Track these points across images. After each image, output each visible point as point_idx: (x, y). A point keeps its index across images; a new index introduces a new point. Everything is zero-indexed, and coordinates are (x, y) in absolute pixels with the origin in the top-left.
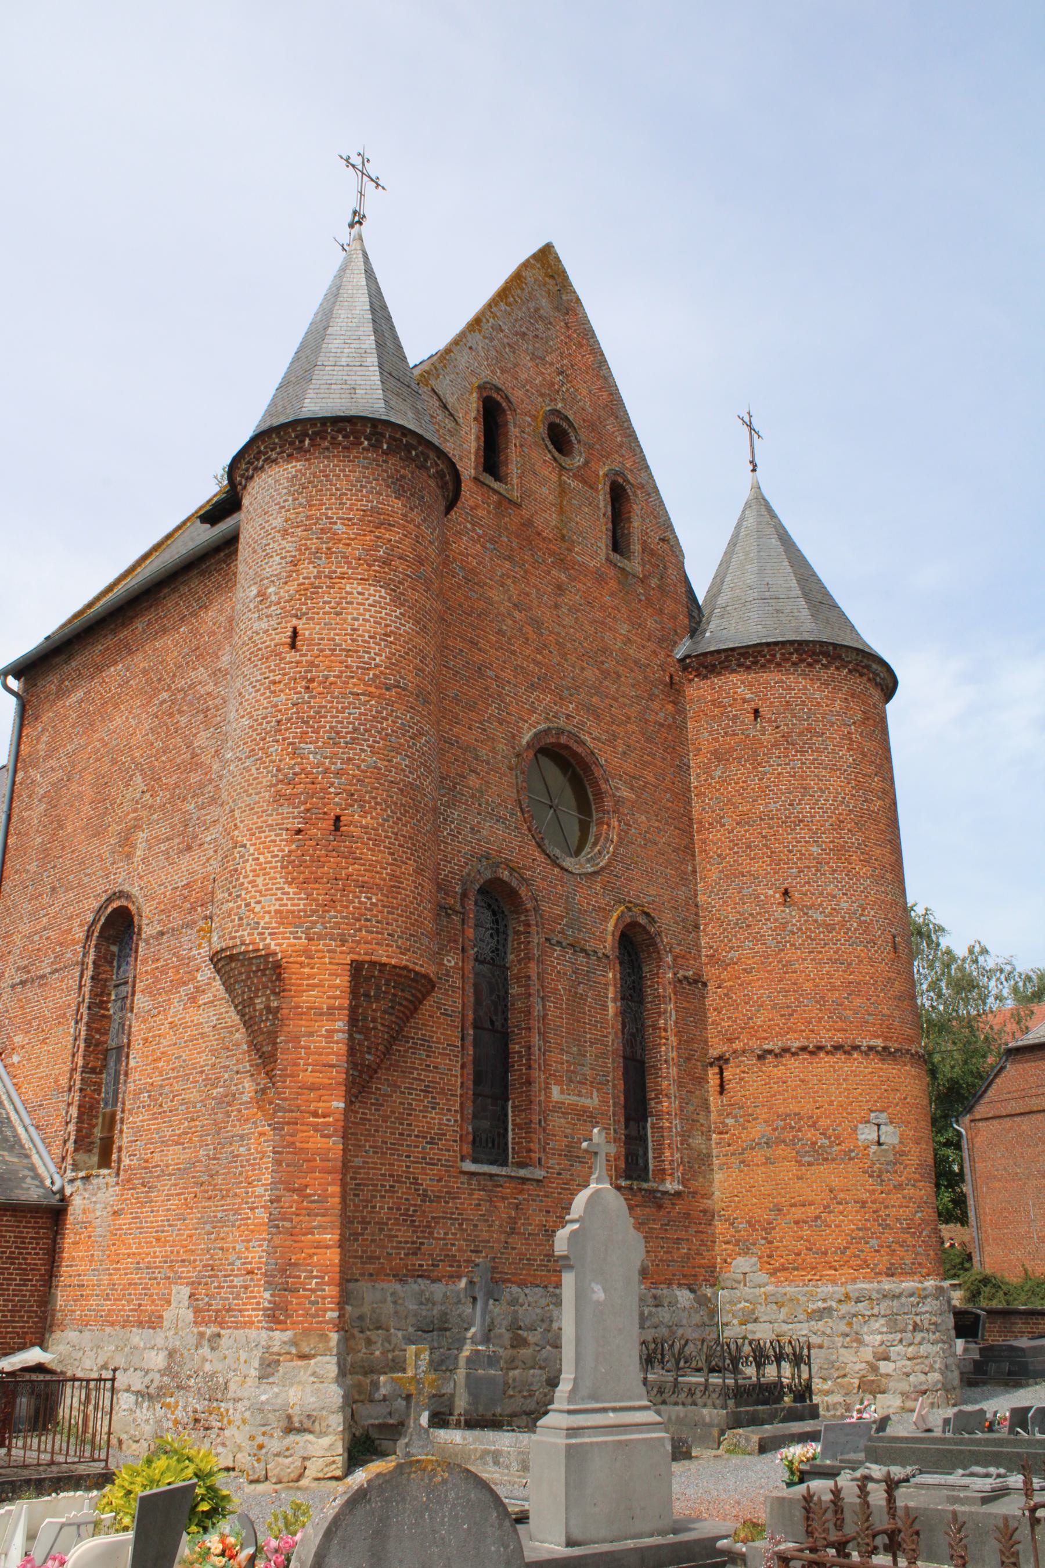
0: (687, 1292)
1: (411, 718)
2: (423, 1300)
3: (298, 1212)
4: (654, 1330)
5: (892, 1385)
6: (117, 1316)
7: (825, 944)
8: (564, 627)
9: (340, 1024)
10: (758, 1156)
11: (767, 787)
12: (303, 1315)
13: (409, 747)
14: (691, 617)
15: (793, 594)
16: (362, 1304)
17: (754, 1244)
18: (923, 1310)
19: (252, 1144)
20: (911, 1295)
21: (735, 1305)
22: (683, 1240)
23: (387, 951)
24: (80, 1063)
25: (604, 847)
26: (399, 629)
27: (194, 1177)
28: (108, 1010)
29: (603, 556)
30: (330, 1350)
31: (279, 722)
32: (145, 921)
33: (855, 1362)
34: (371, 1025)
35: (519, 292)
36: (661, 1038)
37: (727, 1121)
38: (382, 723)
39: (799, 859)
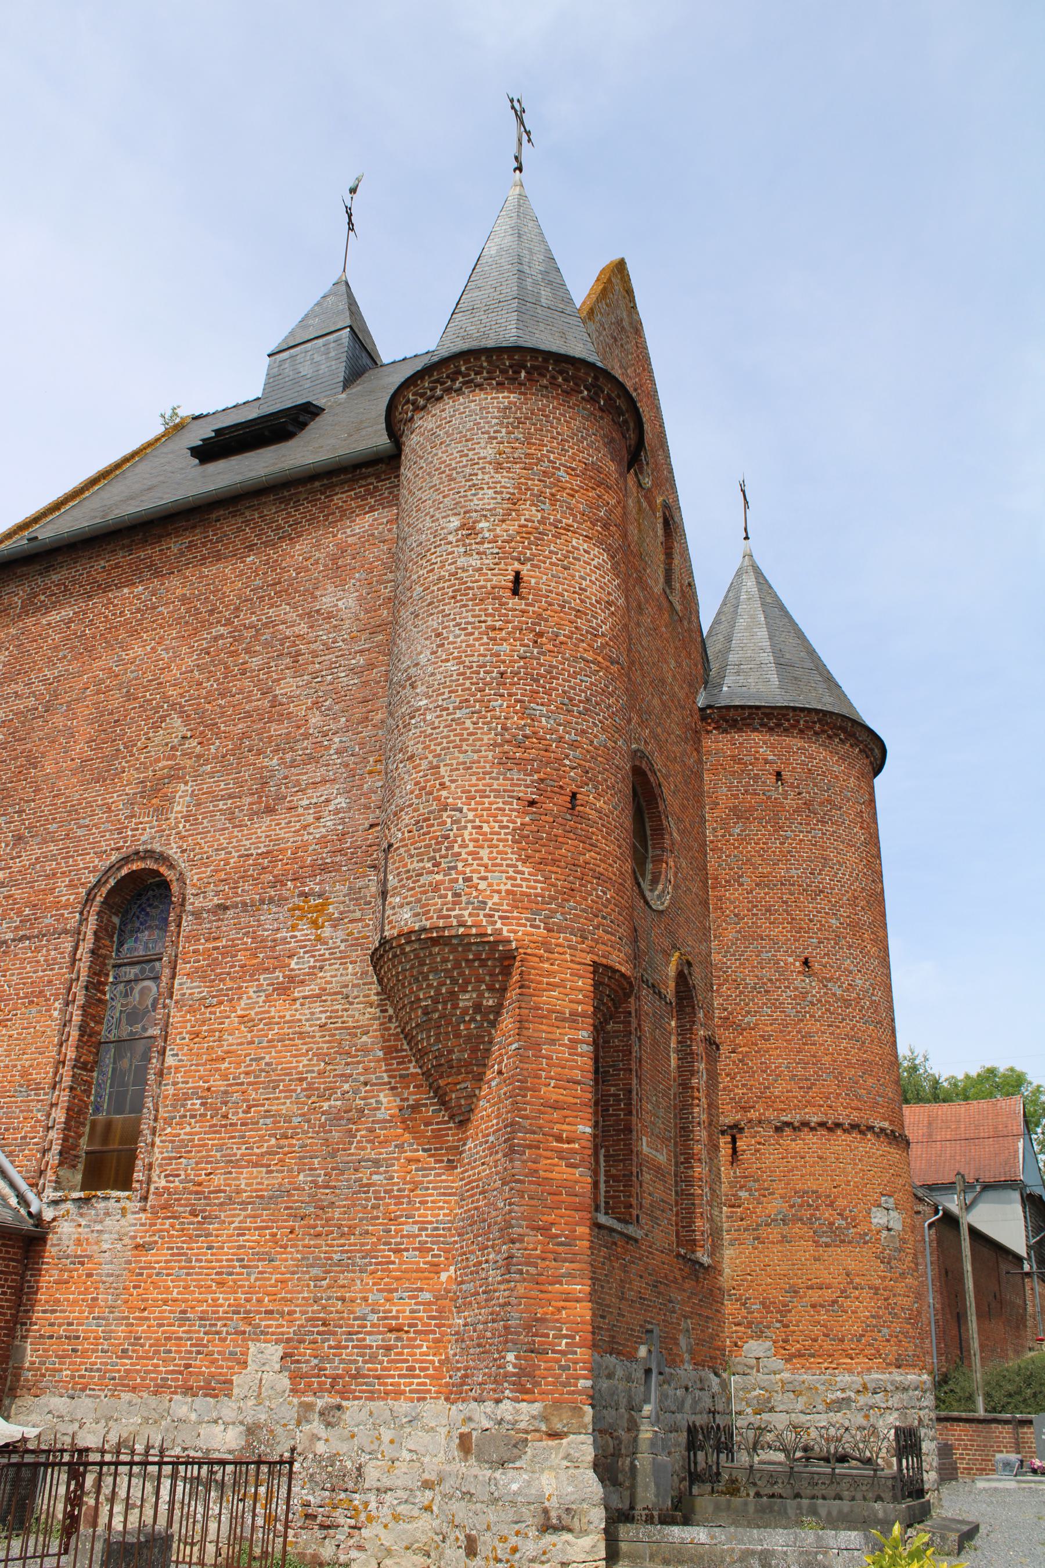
3: (544, 1255)
6: (143, 1379)
9: (585, 1034)
10: (774, 1233)
11: (789, 852)
12: (553, 1384)
17: (769, 1327)
18: (925, 1404)
19: (396, 1172)
20: (916, 1389)
21: (749, 1392)
24: (71, 1054)
25: (665, 888)
27: (287, 1208)
28: (105, 994)
30: (585, 1427)
31: (502, 674)
32: (190, 890)
36: (693, 1098)
39: (819, 929)
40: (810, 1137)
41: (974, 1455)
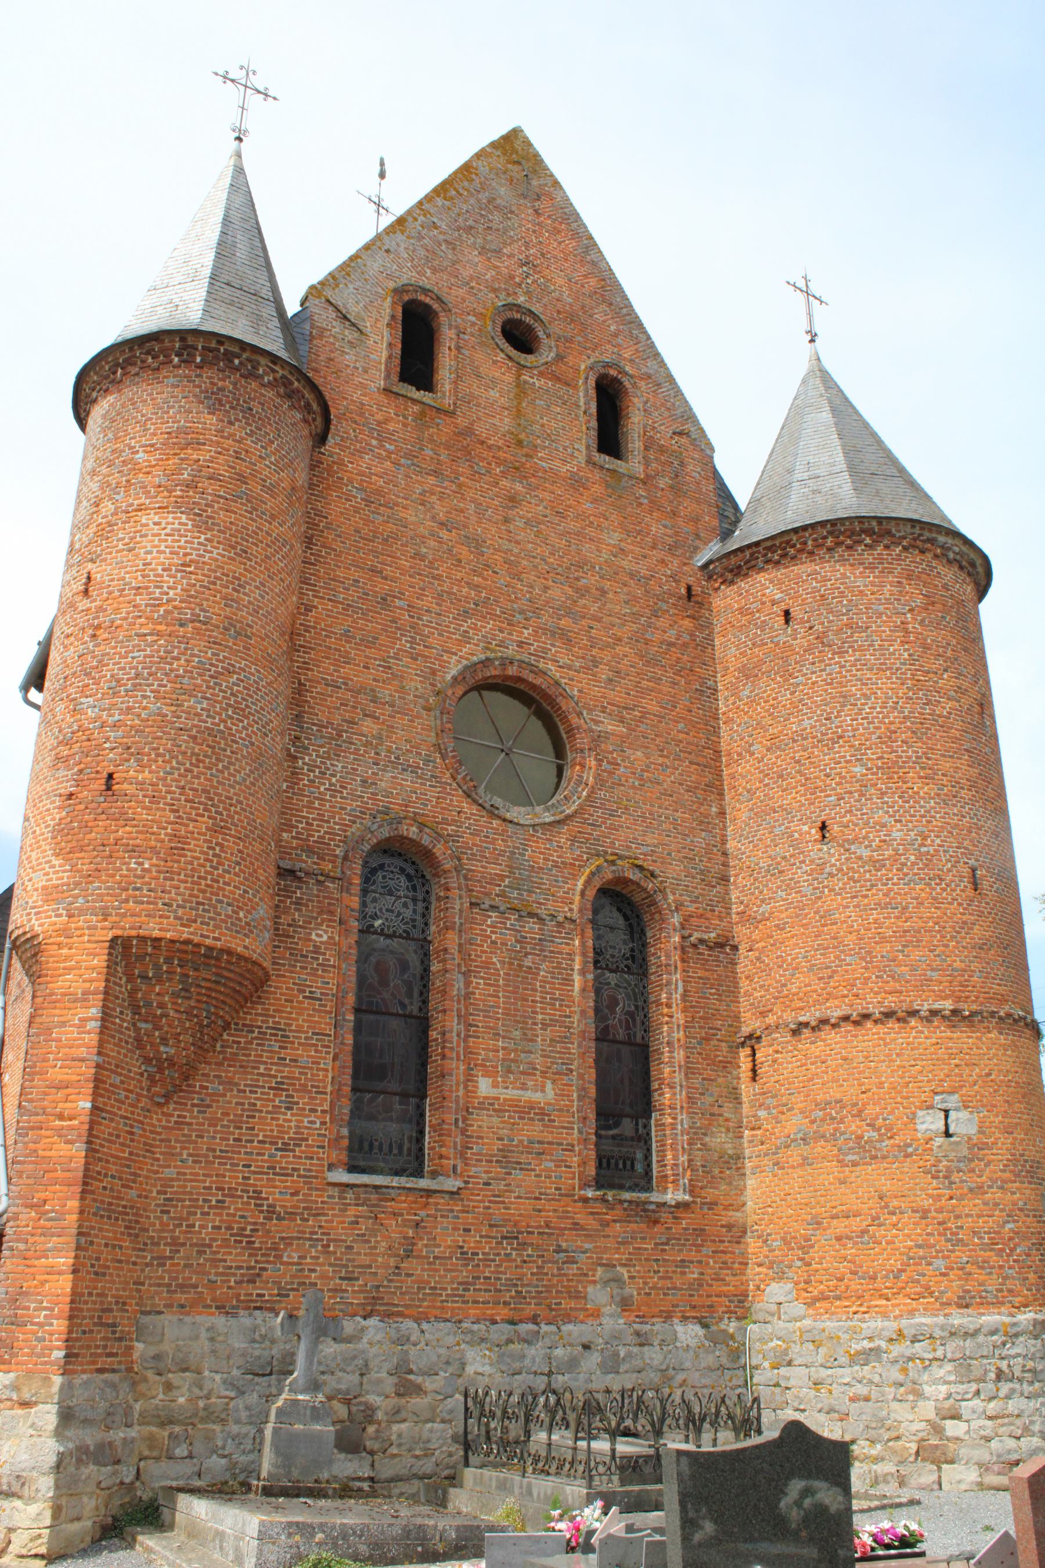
1: (213, 654)
2: (257, 1337)
4: (635, 1375)
5: (963, 1451)
7: (872, 886)
8: (518, 543)
10: (794, 1155)
11: (800, 701)
12: (28, 1355)
13: (208, 687)
14: (722, 516)
15: (837, 469)
16: (161, 1341)
18: (1012, 1352)
21: (766, 1343)
22: (692, 1262)
23: (161, 923)
26: (203, 556)
29: (582, 458)
30: (51, 1396)
33: (912, 1420)
34: (159, 1012)
35: (466, 184)
36: (663, 1015)
38: (171, 664)
40: (831, 1036)
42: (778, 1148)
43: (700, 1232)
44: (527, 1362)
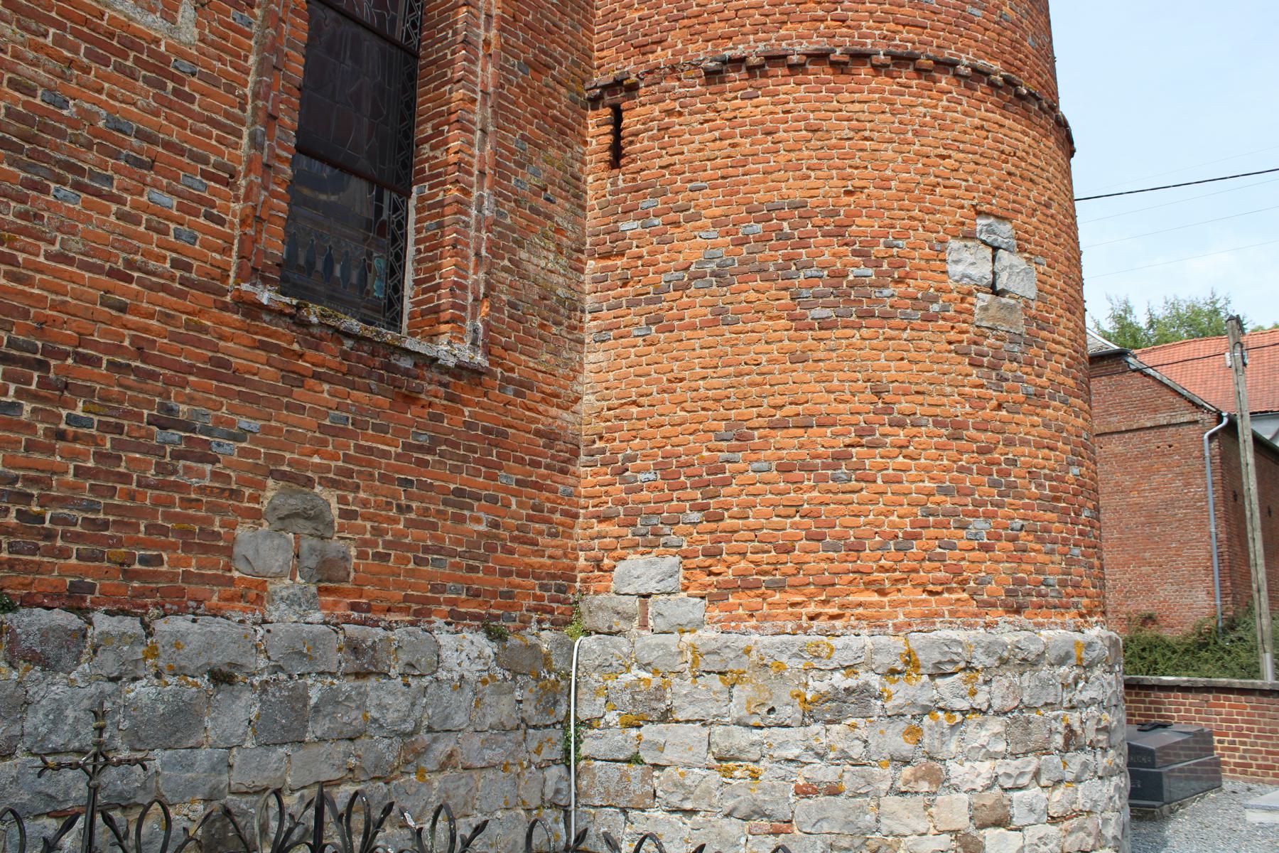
0: (480, 639)
4: (343, 746)
10: (698, 305)
18: (1086, 696)
20: (1061, 661)
22: (478, 498)
37: (623, 226)
40: (788, 88)
41: (1253, 744)
42: (659, 291)
43: (496, 436)
44: (35, 721)
